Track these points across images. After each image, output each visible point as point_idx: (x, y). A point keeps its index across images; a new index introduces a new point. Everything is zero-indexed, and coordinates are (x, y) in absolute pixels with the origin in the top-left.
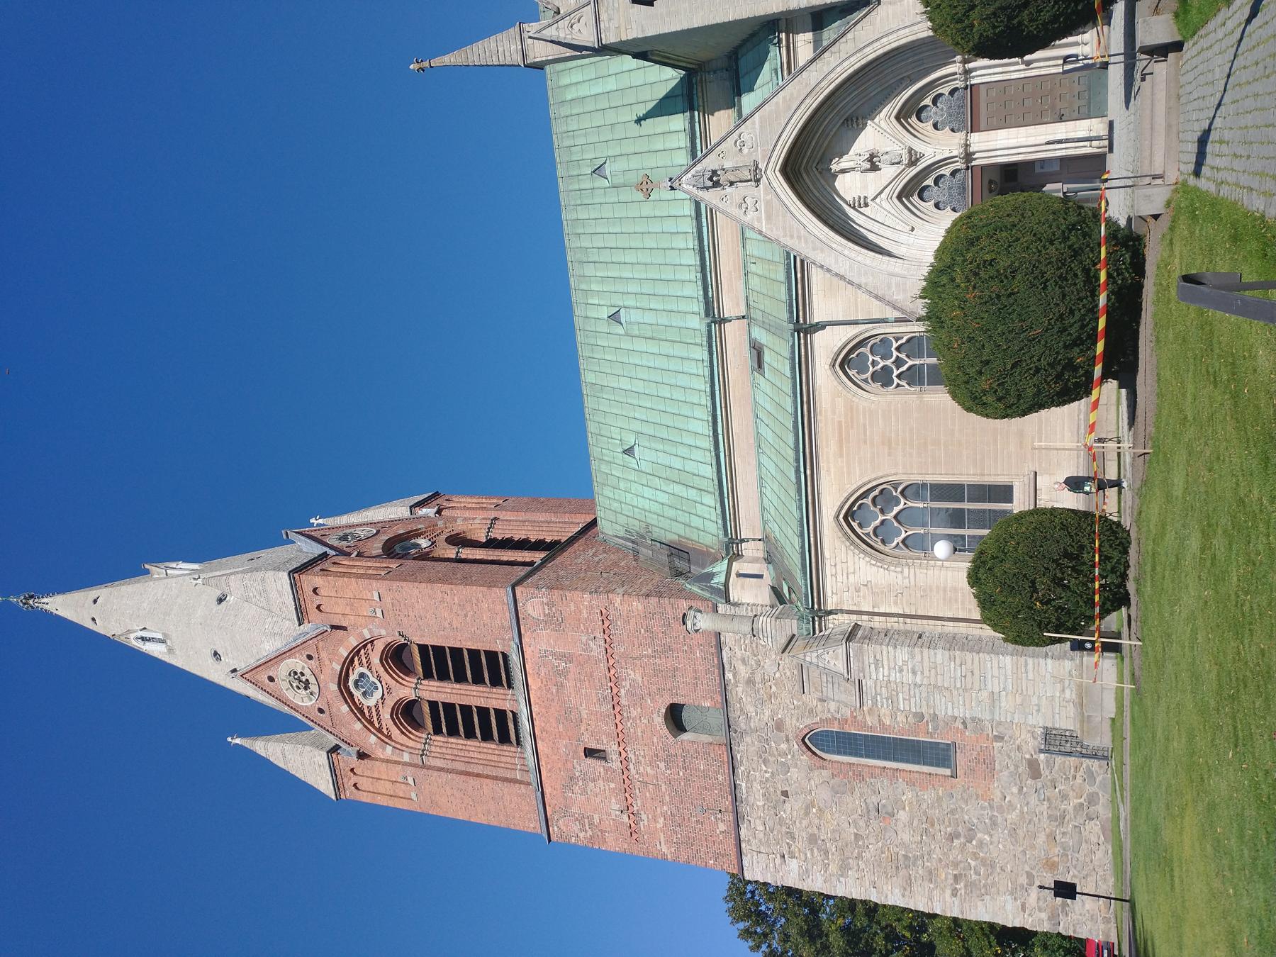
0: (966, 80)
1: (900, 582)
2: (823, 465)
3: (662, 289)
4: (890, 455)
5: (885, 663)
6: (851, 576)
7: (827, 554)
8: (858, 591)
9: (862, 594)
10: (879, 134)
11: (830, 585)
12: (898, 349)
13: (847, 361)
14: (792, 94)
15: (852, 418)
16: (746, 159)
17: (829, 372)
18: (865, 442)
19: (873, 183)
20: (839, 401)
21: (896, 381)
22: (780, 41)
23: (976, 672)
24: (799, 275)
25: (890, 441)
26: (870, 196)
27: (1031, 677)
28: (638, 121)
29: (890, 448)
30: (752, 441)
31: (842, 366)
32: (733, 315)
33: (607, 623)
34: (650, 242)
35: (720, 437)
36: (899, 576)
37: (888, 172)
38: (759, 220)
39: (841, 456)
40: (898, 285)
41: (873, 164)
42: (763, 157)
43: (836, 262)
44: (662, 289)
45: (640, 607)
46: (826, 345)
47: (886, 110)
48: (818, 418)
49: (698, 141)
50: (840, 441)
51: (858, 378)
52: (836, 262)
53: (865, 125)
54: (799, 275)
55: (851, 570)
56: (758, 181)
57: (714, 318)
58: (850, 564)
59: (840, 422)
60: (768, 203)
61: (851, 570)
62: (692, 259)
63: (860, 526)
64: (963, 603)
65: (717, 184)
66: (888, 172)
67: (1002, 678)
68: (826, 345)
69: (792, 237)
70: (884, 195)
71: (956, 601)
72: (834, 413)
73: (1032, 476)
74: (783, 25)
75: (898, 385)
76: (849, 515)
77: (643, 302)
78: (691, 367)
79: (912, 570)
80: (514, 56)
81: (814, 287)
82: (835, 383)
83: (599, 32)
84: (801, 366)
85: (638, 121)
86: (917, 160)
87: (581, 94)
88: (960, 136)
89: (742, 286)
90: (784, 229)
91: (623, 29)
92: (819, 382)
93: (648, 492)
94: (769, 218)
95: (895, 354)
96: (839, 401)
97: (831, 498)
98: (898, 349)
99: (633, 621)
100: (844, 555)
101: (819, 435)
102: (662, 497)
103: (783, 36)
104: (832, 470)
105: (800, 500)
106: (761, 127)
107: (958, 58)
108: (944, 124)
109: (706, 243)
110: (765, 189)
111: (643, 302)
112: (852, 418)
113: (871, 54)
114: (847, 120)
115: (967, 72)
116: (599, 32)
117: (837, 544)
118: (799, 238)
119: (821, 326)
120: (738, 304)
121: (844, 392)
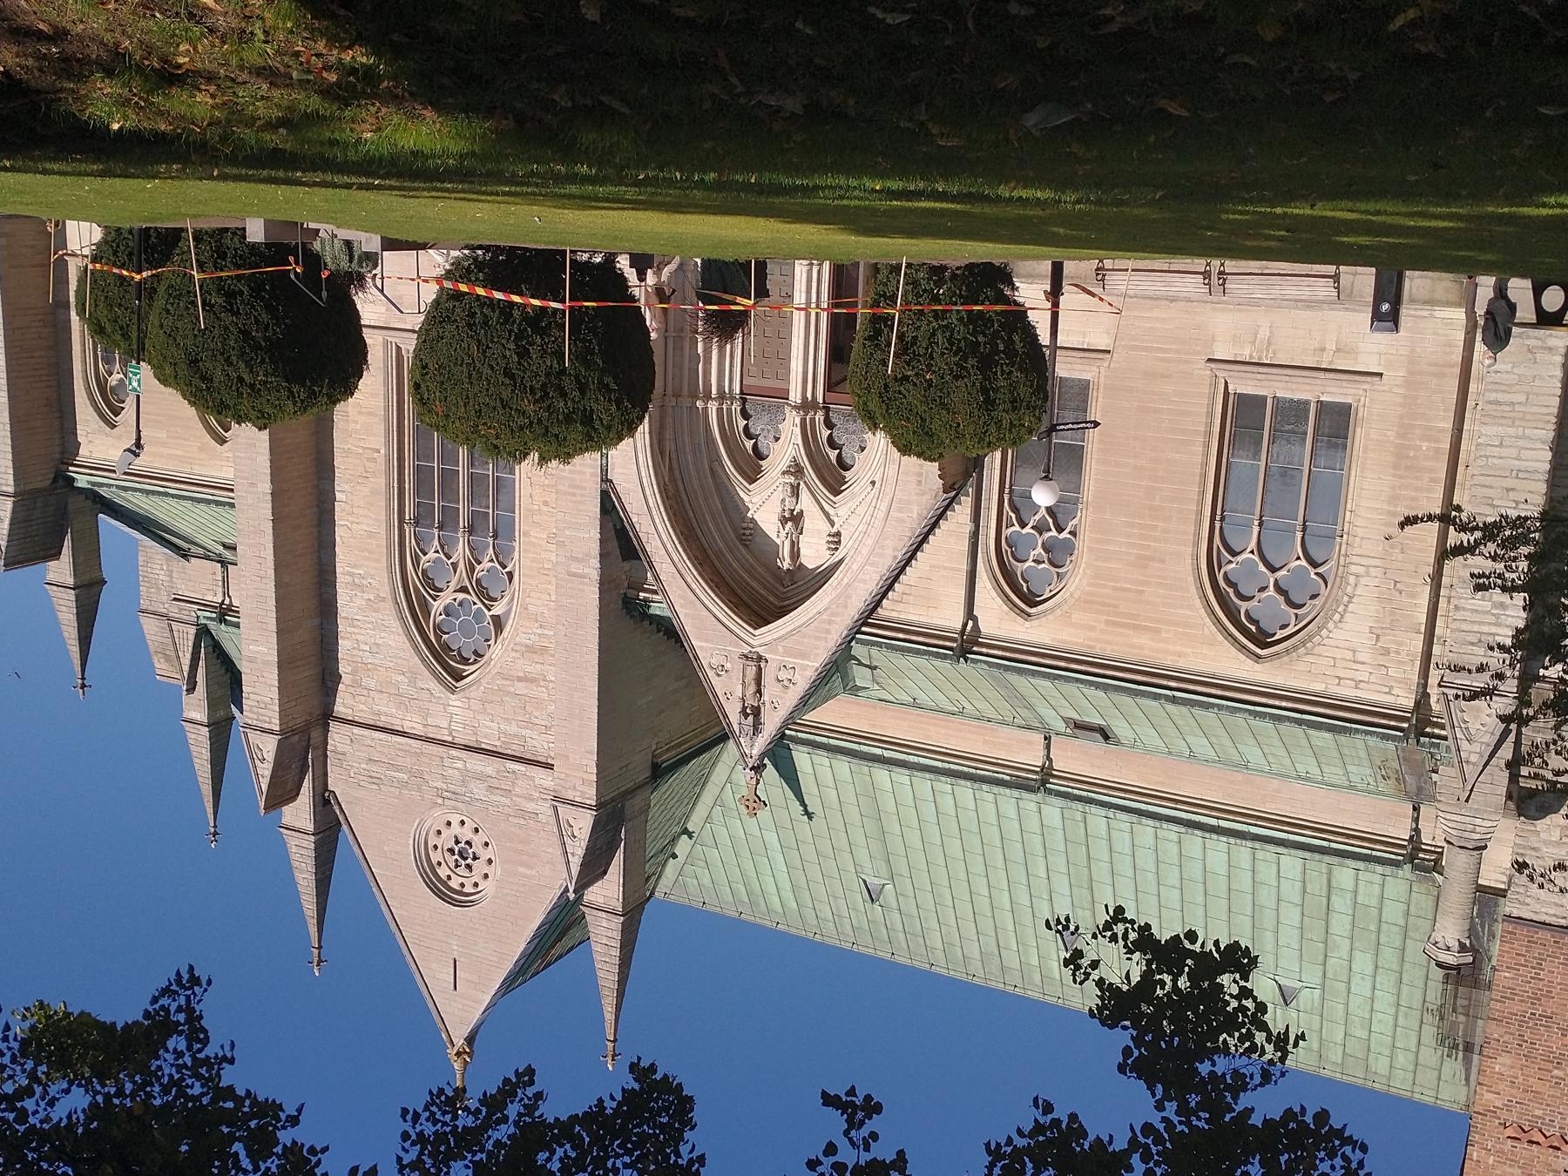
0: (732, 398)
1: (1373, 582)
2: (1168, 661)
3: (1016, 852)
4: (1163, 561)
5: (1485, 629)
6: (1360, 657)
7: (1318, 687)
8: (1387, 652)
9: (1393, 647)
10: (764, 505)
11: (1371, 694)
12: (1023, 525)
13: (1026, 598)
14: (680, 597)
15: (1103, 605)
16: (734, 666)
17: (1035, 623)
18: (1141, 592)
19: (814, 523)
20: (1076, 617)
21: (1065, 535)
22: (646, 600)
23: (1509, 483)
24: (901, 636)
25: (1141, 557)
26: (826, 528)
27: (1522, 398)
28: (810, 815)
29: (1152, 559)
30: (1240, 777)
31: (1264, 645)
32: (1042, 753)
33: (1538, 1137)
34: (955, 847)
35: (887, 754)
36: (1363, 581)
37: (806, 502)
38: (804, 668)
39: (1157, 631)
40: (900, 510)
41: (794, 519)
42: (737, 646)
43: (864, 582)
44: (1016, 852)
45: (1506, 1059)
46: (997, 618)
47: (742, 494)
48: (1098, 651)
49: (818, 739)
50: (1135, 627)
51: (1055, 588)
52: (864, 582)
53: (753, 520)
54: (901, 636)
55: (1349, 655)
56: (760, 658)
57: (1042, 781)
58: (1338, 654)
59: (1107, 622)
60: (787, 652)
61: (1349, 655)
62: (965, 790)
63: (1283, 627)
64: (1417, 489)
65: (757, 712)
66: (806, 502)
67: (1521, 443)
68: (997, 618)
69: (828, 632)
70: (831, 512)
71: (1414, 499)
72: (1092, 628)
73: (1213, 365)
74: (631, 593)
75: (1073, 533)
76: (1262, 639)
77: (1040, 885)
78: (1369, 895)
79: (1355, 559)
80: (613, 926)
81: (924, 620)
82: (1051, 617)
83: (582, 806)
84: (1019, 659)
85: (810, 815)
86: (797, 465)
87: (788, 886)
88: (787, 410)
89: (1006, 730)
90: (818, 639)
91: (585, 776)
92: (1047, 641)
93: (1361, 988)
94: (803, 655)
95: (1028, 530)
96: (1076, 617)
97: (1227, 661)
98: (1023, 525)
99: (1537, 1086)
100: (1321, 661)
101: (1128, 657)
102: (1363, 963)
103: (642, 595)
104: (1178, 648)
105: (1220, 707)
106: (706, 641)
107: (699, 404)
108: (778, 430)
109: (939, 764)
110: (772, 652)
111: (1040, 885)
112: (1103, 605)
113: (655, 500)
114: (741, 540)
115: (722, 396)
116: (582, 806)
117: (1301, 666)
118: (830, 622)
119: (1422, 700)
120: (1029, 743)
121: (1065, 608)
